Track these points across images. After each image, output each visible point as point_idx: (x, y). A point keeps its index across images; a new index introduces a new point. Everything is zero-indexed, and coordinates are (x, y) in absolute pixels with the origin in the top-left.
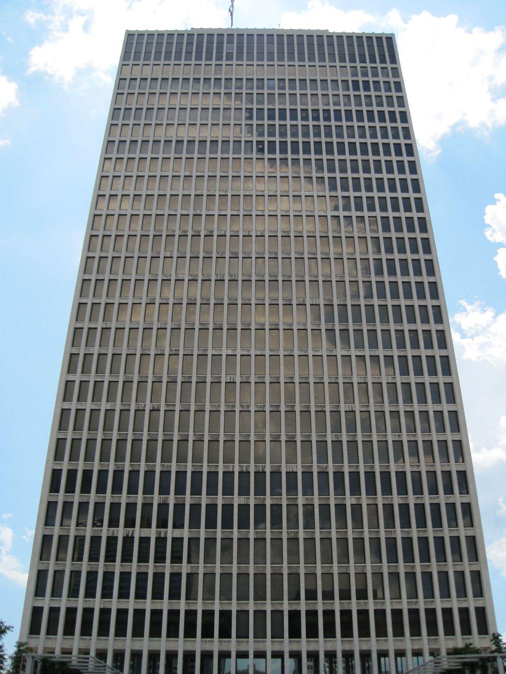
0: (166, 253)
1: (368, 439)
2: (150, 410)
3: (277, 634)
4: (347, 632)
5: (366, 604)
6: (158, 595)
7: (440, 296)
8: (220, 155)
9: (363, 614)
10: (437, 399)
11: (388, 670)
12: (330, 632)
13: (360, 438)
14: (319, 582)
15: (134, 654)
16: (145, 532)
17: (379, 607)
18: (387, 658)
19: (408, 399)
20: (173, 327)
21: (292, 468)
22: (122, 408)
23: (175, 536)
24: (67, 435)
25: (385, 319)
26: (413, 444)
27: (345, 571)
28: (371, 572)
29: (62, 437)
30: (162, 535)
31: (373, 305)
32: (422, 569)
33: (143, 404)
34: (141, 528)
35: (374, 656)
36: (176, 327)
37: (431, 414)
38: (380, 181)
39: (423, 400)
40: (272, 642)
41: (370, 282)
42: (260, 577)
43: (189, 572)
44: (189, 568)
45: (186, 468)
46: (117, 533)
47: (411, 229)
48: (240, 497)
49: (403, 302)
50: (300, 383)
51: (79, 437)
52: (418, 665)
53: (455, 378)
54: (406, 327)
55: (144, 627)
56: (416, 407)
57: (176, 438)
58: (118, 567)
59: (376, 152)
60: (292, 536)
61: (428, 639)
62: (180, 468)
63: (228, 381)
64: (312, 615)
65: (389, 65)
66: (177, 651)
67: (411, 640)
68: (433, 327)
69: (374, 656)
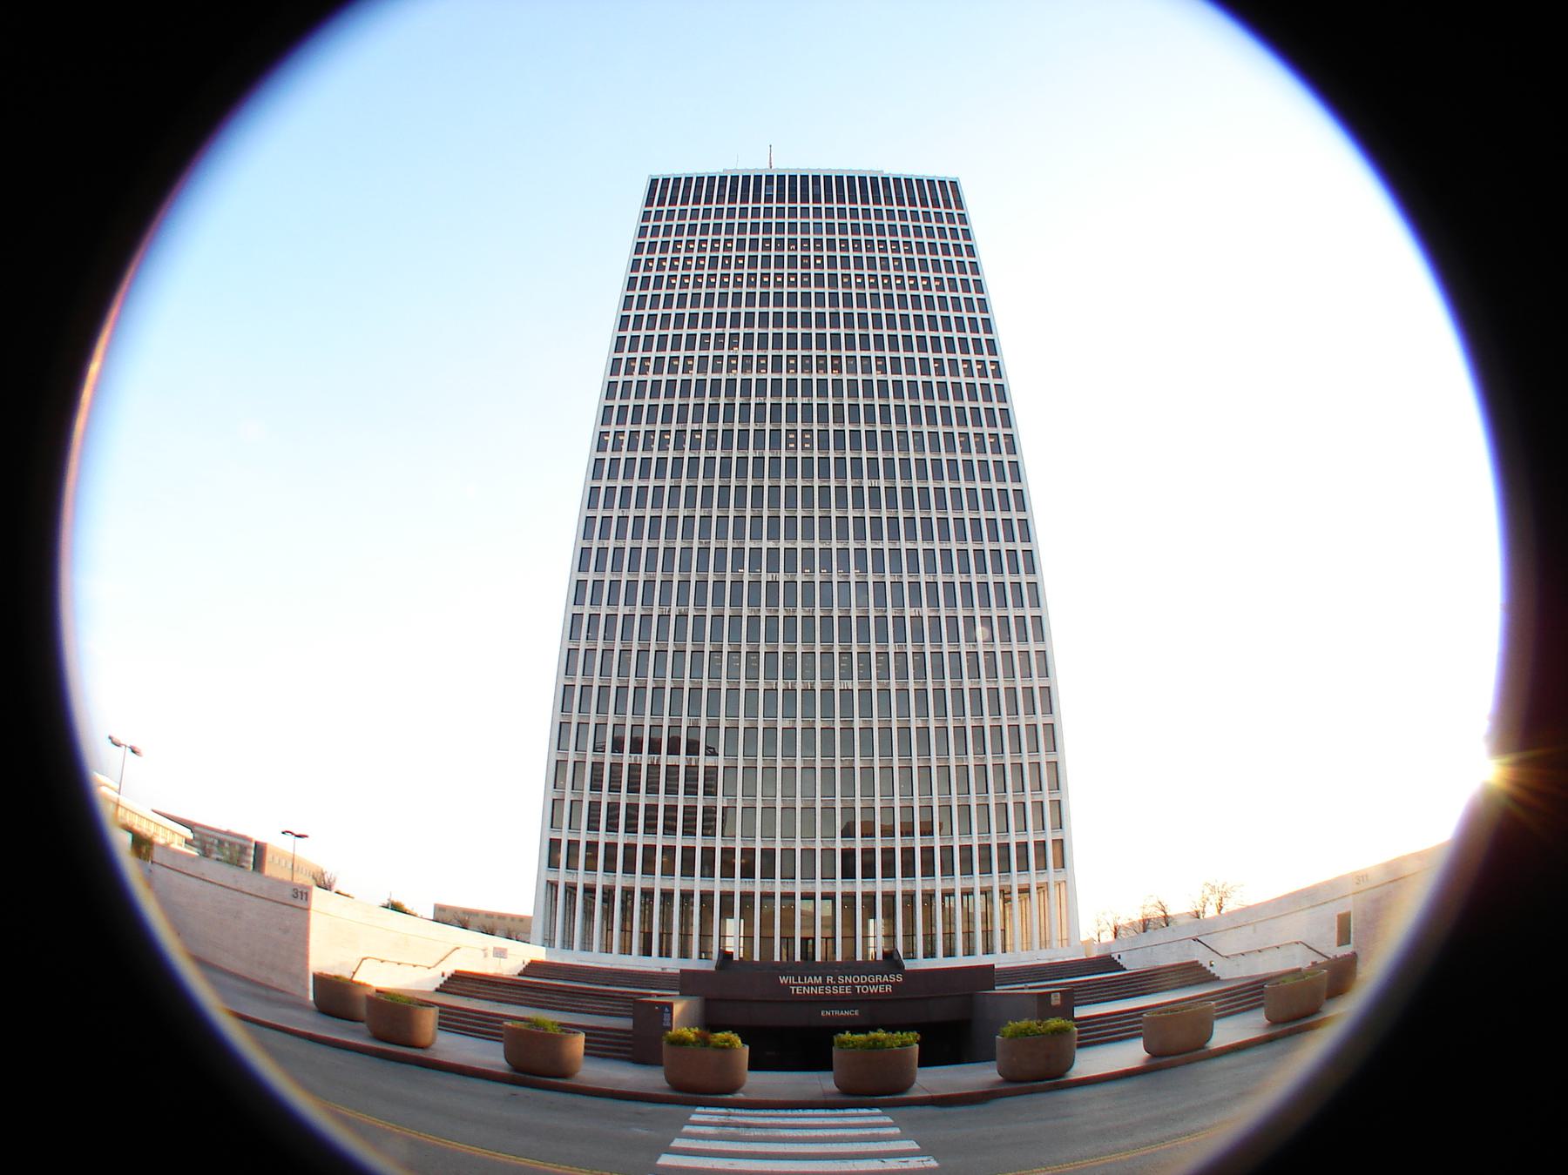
0: (694, 425)
6: (689, 830)
7: (1037, 571)
9: (928, 852)
10: (1015, 570)
11: (588, 923)
12: (888, 872)
14: (878, 818)
15: (646, 893)
18: (952, 898)
20: (703, 515)
22: (643, 613)
26: (863, 317)
28: (938, 804)
29: (574, 647)
30: (693, 764)
31: (944, 489)
32: (996, 800)
34: (668, 754)
35: (938, 896)
37: (1012, 620)
43: (726, 805)
44: (725, 800)
45: (720, 685)
49: (971, 430)
50: (856, 582)
52: (1219, 911)
53: (1039, 577)
58: (643, 799)
60: (847, 764)
61: (1000, 876)
62: (713, 685)
64: (868, 853)
66: (673, 890)
67: (980, 877)
68: (1010, 486)
69: (938, 896)
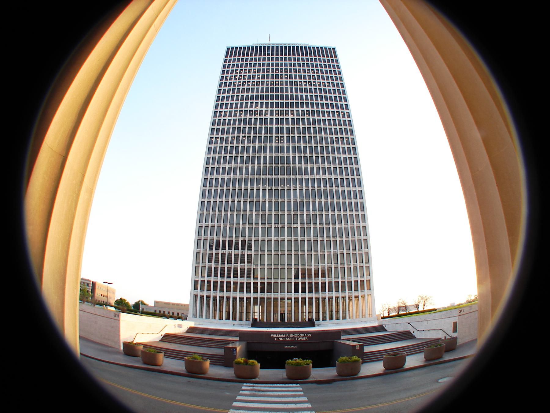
1: (327, 214)
2: (237, 202)
3: (290, 292)
4: (317, 291)
5: (325, 280)
8: (268, 126)
9: (324, 283)
13: (318, 213)
16: (236, 252)
17: (330, 281)
19: (344, 197)
21: (296, 225)
23: (248, 254)
24: (204, 212)
25: (335, 163)
27: (317, 267)
30: (243, 253)
33: (234, 199)
36: (247, 166)
38: (332, 104)
39: (344, 197)
40: (287, 294)
41: (329, 147)
42: (283, 284)
46: (225, 252)
47: (345, 125)
48: (261, 293)
51: (209, 213)
54: (343, 166)
55: (390, 16)
56: (347, 200)
57: (248, 213)
58: (226, 266)
59: (330, 93)
60: (296, 253)
62: (250, 226)
63: (269, 189)
64: (303, 284)
65: (334, 59)
